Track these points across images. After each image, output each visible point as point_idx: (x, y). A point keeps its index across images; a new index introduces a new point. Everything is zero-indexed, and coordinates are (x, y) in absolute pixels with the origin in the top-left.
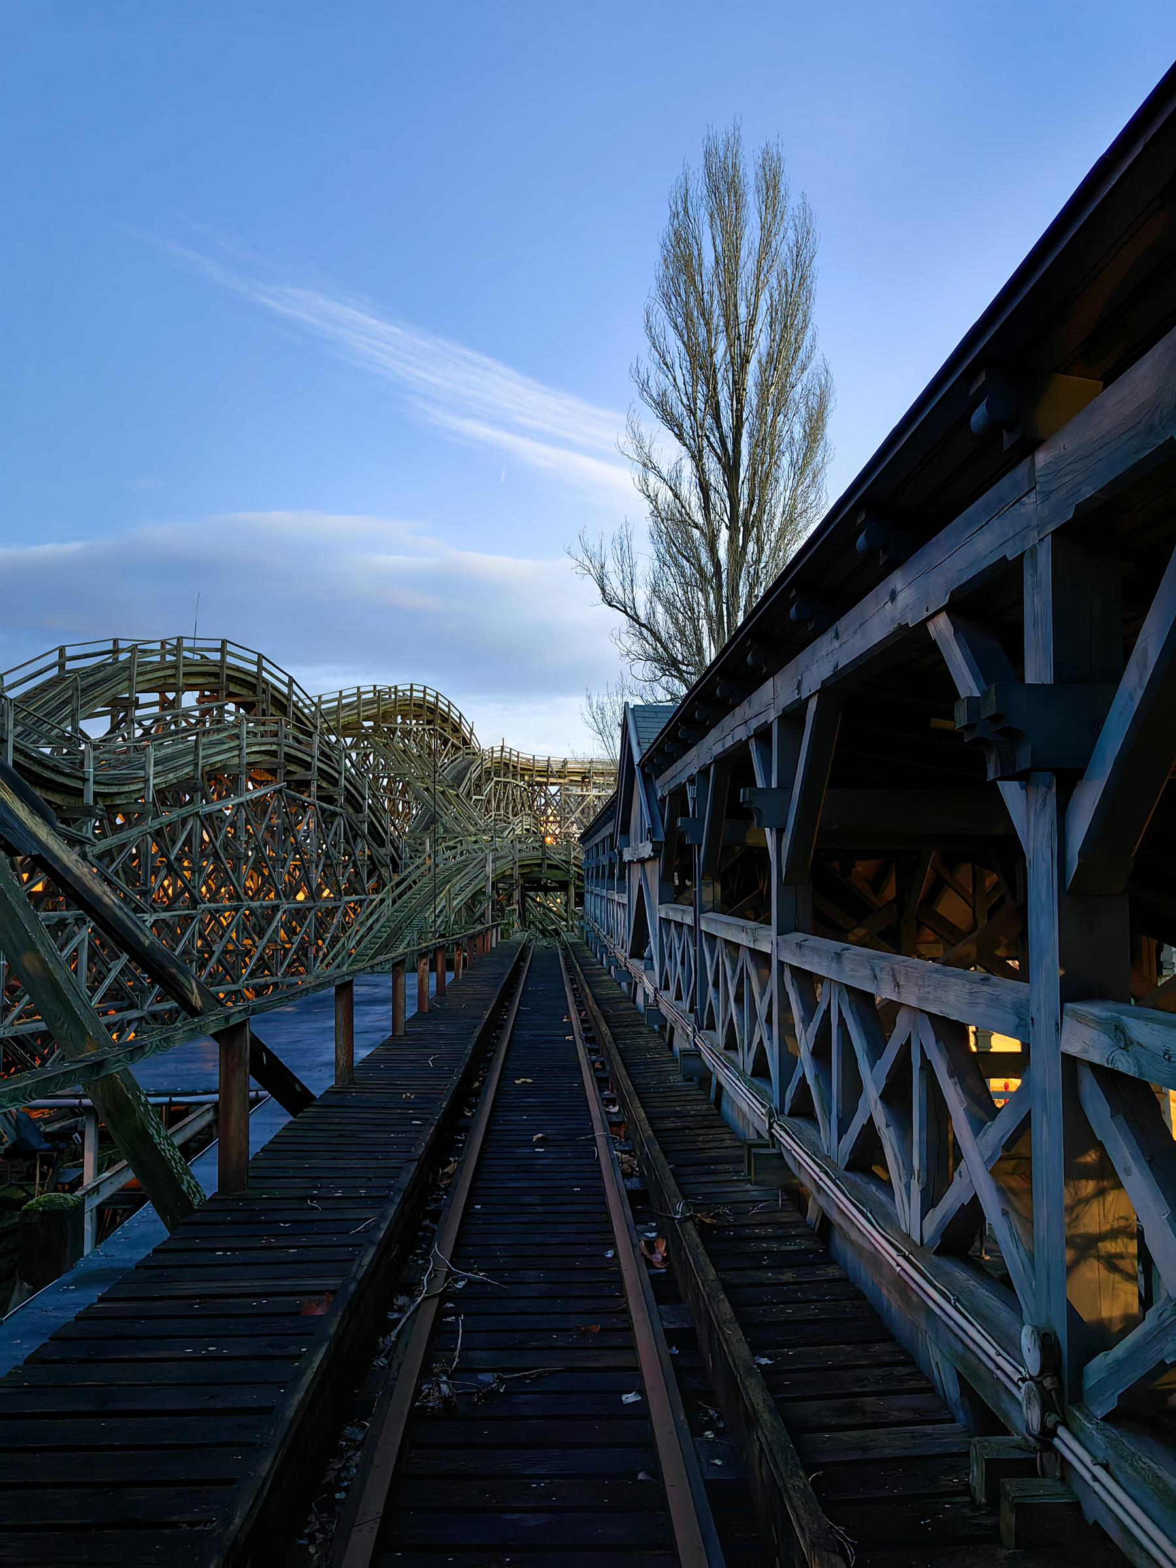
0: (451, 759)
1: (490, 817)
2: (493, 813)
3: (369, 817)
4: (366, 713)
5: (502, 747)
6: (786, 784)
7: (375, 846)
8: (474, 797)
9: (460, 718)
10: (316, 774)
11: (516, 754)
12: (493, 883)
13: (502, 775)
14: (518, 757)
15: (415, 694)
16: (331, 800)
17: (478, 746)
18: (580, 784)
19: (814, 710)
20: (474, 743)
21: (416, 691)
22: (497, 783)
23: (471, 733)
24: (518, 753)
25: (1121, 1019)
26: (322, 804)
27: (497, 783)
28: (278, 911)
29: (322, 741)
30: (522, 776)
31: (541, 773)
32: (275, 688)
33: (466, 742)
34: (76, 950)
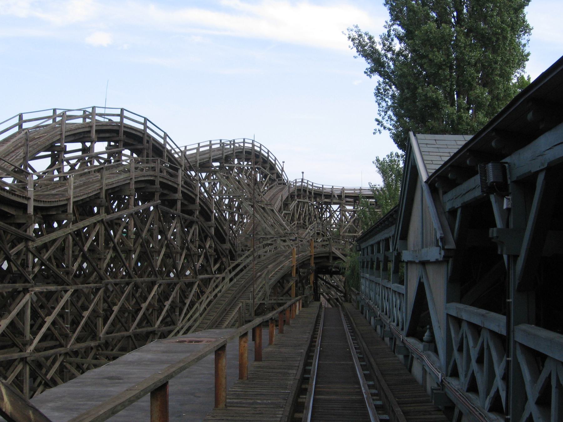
0: (269, 187)
1: (294, 224)
2: (296, 222)
3: (215, 224)
4: (215, 157)
5: (302, 179)
7: (219, 242)
8: (284, 212)
9: (268, 153)
10: (181, 195)
12: (297, 269)
15: (246, 145)
17: (286, 179)
20: (284, 177)
22: (298, 202)
23: (282, 170)
24: (313, 183)
26: (184, 215)
27: (298, 202)
28: (155, 284)
29: (185, 174)
32: (154, 140)
33: (279, 176)
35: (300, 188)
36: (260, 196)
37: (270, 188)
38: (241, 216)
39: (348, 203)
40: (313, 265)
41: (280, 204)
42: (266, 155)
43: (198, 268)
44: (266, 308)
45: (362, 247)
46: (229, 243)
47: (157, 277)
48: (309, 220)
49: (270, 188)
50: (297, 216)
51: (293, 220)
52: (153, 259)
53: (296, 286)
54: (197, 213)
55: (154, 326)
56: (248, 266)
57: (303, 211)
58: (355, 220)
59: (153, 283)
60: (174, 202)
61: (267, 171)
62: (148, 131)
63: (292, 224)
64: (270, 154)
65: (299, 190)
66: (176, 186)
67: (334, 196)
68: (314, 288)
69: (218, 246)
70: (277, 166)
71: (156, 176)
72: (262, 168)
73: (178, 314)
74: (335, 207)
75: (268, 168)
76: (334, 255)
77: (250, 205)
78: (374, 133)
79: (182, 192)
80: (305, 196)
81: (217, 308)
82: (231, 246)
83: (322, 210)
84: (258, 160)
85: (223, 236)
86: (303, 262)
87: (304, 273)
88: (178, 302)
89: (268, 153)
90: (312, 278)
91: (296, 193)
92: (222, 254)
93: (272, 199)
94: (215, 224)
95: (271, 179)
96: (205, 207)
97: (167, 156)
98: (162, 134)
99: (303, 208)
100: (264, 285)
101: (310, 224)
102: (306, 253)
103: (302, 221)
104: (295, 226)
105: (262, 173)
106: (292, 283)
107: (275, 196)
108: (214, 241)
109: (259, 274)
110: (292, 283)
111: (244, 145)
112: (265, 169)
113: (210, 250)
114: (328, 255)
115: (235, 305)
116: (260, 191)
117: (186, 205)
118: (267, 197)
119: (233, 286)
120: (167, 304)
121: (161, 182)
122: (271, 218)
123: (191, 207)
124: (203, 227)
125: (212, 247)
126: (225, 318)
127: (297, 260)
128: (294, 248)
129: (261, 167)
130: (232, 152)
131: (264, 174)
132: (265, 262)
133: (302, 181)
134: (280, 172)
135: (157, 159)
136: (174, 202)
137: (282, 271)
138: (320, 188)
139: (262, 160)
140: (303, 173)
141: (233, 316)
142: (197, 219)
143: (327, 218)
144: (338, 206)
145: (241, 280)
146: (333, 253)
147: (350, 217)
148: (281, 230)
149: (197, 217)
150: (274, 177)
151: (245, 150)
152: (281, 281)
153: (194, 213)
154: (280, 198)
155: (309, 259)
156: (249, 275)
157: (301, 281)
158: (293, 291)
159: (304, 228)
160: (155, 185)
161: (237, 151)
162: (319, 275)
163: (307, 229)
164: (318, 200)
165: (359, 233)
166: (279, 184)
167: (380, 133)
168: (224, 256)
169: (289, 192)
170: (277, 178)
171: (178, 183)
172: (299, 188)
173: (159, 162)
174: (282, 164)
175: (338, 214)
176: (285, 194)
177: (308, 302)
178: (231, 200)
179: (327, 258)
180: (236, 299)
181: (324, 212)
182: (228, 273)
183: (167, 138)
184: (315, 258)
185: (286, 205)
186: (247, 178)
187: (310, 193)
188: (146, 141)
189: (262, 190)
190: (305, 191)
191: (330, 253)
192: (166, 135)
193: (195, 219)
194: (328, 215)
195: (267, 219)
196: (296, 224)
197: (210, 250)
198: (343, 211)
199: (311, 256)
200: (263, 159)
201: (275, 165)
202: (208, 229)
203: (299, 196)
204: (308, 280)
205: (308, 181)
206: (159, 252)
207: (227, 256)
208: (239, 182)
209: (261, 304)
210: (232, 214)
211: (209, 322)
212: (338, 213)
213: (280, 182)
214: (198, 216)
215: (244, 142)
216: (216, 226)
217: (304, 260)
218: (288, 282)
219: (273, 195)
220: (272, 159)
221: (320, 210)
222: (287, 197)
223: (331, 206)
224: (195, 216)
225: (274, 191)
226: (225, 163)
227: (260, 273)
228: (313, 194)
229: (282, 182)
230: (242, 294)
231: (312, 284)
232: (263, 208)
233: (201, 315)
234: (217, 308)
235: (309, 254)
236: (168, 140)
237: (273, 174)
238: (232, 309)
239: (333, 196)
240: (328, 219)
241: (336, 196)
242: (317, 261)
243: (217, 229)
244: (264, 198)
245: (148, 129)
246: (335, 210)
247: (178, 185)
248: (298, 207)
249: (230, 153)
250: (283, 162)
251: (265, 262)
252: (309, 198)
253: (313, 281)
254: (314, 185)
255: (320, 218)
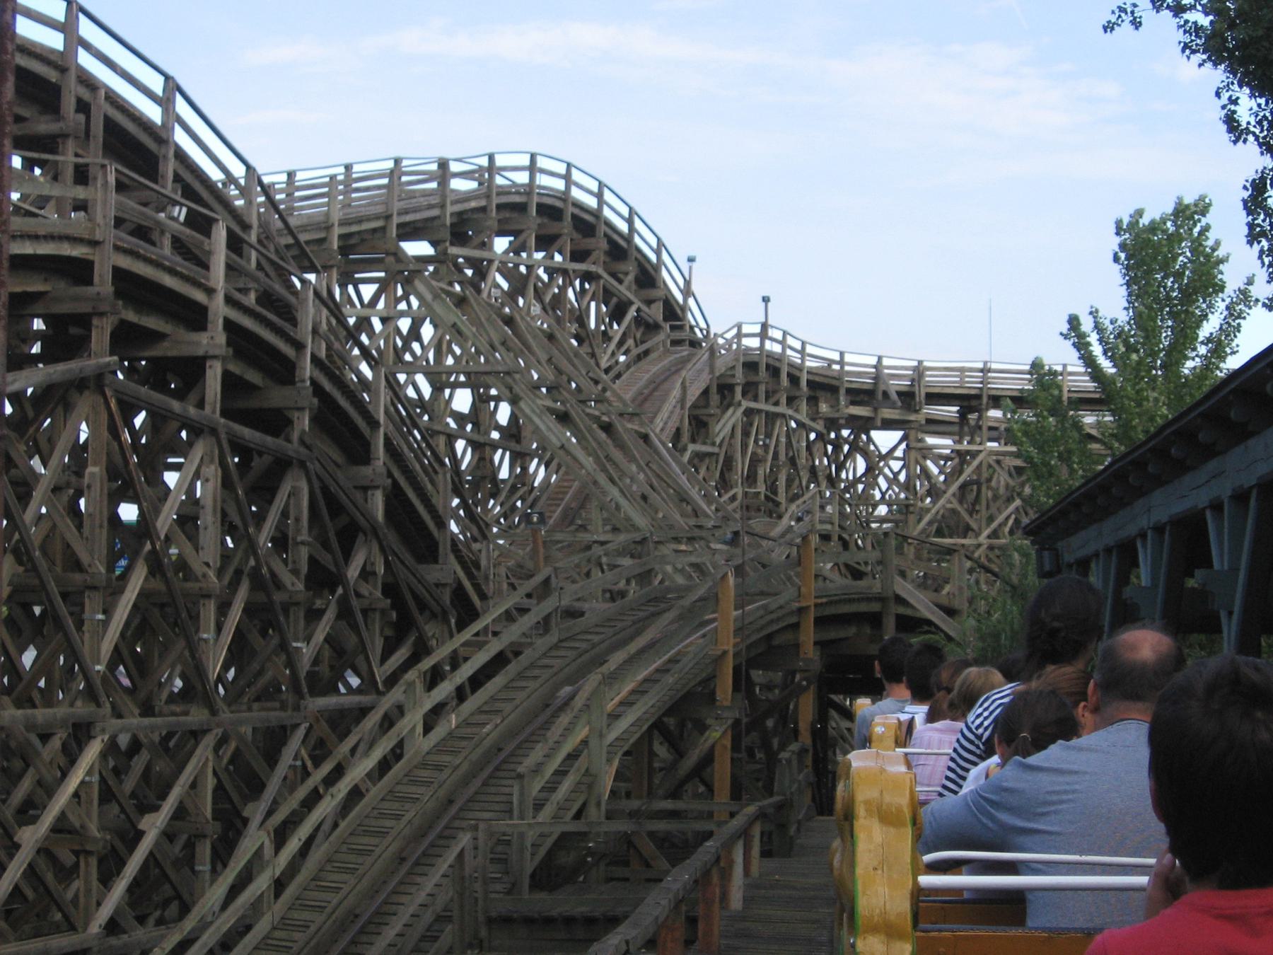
0: (635, 352)
1: (733, 498)
2: (738, 490)
3: (390, 475)
4: (408, 218)
5: (765, 326)
6: (1234, 569)
7: (408, 558)
8: (691, 448)
9: (630, 221)
10: (221, 338)
11: (798, 345)
12: (736, 670)
13: (762, 396)
14: (802, 352)
15: (543, 180)
16: (276, 422)
17: (703, 325)
18: (956, 428)
19: (948, 722)
20: (694, 316)
21: (543, 171)
22: (749, 413)
23: (687, 291)
24: (804, 344)
25: (452, 601)
26: (231, 424)
27: (749, 413)
28: (90, 737)
29: (264, 262)
30: (813, 401)
31: (861, 395)
32: (113, 99)
33: (674, 313)
34: (193, 785)
35: (756, 359)
36: (596, 382)
37: (639, 358)
38: (519, 458)
39: (935, 426)
40: (810, 651)
41: (675, 417)
42: (623, 227)
43: (305, 664)
44: (590, 852)
45: (1068, 558)
46: (452, 558)
47: (98, 705)
48: (789, 485)
49: (639, 358)
50: (741, 466)
51: (724, 484)
52: (80, 624)
53: (736, 747)
54: (303, 422)
55: (86, 925)
56: (517, 654)
57: (766, 446)
58: (963, 487)
59: (81, 733)
60: (192, 370)
61: (625, 290)
62: (85, 60)
63: (726, 497)
64: (638, 224)
65: (751, 366)
66: (199, 296)
67: (885, 394)
68: (815, 754)
69: (402, 573)
70: (664, 274)
71: (94, 244)
72: (605, 275)
73: (207, 867)
74: (884, 439)
75: (631, 277)
76: (902, 610)
77: (551, 411)
78: (1109, 27)
79: (229, 325)
80: (775, 392)
81: (360, 853)
82: (461, 574)
83: (837, 447)
84: (589, 243)
85: (426, 528)
86: (769, 637)
87: (768, 687)
88: (208, 813)
89: (630, 221)
90: (806, 708)
91: (739, 377)
92: (423, 606)
93: (646, 399)
94: (390, 475)
95: (647, 327)
96: (343, 402)
97: (177, 178)
98: (156, 83)
99: (768, 435)
100: (585, 742)
101: (792, 499)
102: (781, 600)
103: (761, 488)
104: (736, 503)
105: (607, 296)
106: (717, 734)
107: (656, 386)
108: (382, 549)
109: (567, 689)
110: (717, 734)
111: (532, 178)
112: (620, 282)
113: (365, 589)
114: (875, 607)
115: (447, 837)
116: (598, 365)
117: (252, 388)
118: (626, 390)
119: (439, 748)
120: (153, 825)
121: (119, 273)
122: (639, 466)
123: (277, 397)
124: (330, 482)
125: (374, 573)
126: (395, 898)
127: (738, 631)
128: (724, 577)
129: (601, 271)
130: (483, 203)
131: (614, 300)
132: (596, 638)
133: (763, 335)
134: (679, 297)
135: (103, 166)
136: (192, 370)
137: (670, 679)
138: (831, 362)
139: (604, 245)
140: (766, 300)
141: (411, 910)
142: (302, 450)
143: (857, 480)
144: (898, 435)
145: (483, 717)
146: (900, 600)
147: (942, 478)
148: (678, 517)
149: (302, 442)
150: (656, 312)
151: (536, 199)
152: (671, 722)
153: (289, 422)
154: (676, 392)
155: (795, 627)
156: (521, 695)
157: (756, 723)
158: (722, 772)
159: (771, 516)
160: (89, 282)
161: (504, 199)
162: (833, 696)
163: (780, 517)
164: (824, 407)
165: (977, 535)
166: (676, 343)
167: (1137, 24)
168: (434, 616)
169: (712, 371)
170: (665, 319)
171: (211, 284)
172: (749, 359)
173: (112, 179)
174: (685, 267)
175: (896, 469)
176: (696, 380)
177: (792, 830)
178: (480, 401)
179: (875, 620)
180: (453, 810)
181: (846, 457)
182: (419, 687)
183: (179, 100)
184: (820, 622)
185: (699, 425)
186: (544, 309)
187: (794, 380)
188: (73, 101)
189: (604, 363)
190: (774, 371)
191: (881, 599)
192: (172, 87)
193: (293, 448)
194: (861, 465)
195: (623, 474)
196: (740, 496)
197: (365, 589)
198: (916, 452)
199: (801, 611)
200: (611, 242)
201: (657, 268)
202: (358, 496)
203: (750, 389)
204: (786, 718)
205: (785, 333)
206: (116, 588)
207: (445, 613)
208: (509, 321)
209: (564, 836)
210: (481, 447)
211: (319, 918)
212: (896, 465)
213: (677, 335)
214: (308, 440)
215: (532, 168)
216: (395, 484)
217: (775, 627)
218: (702, 728)
219: (651, 381)
220: (645, 243)
221: (830, 448)
222: (706, 392)
223: (870, 439)
224: (295, 436)
225: (652, 368)
226: (452, 244)
227: (567, 689)
228: (804, 383)
229: (684, 335)
230: (485, 784)
231: (806, 738)
232: (607, 428)
233: (279, 885)
234: (360, 853)
235: (796, 605)
236: (181, 107)
237: (649, 302)
238: (425, 861)
239: (880, 396)
240: (860, 487)
241: (894, 396)
242: (833, 634)
243: (395, 498)
244: (615, 393)
245: (82, 53)
246: (884, 451)
247: (210, 291)
248: (746, 434)
249: (473, 204)
250: (691, 260)
251: (596, 638)
252: (791, 400)
253: (813, 725)
254: (809, 349)
255: (832, 481)
